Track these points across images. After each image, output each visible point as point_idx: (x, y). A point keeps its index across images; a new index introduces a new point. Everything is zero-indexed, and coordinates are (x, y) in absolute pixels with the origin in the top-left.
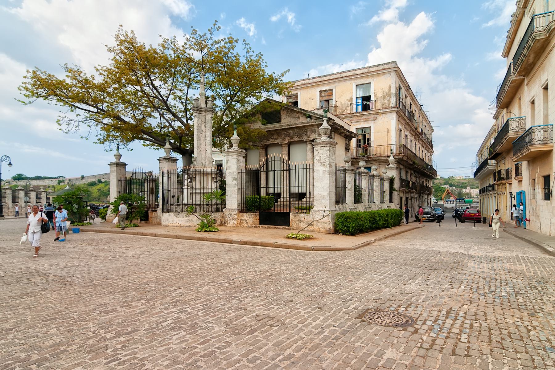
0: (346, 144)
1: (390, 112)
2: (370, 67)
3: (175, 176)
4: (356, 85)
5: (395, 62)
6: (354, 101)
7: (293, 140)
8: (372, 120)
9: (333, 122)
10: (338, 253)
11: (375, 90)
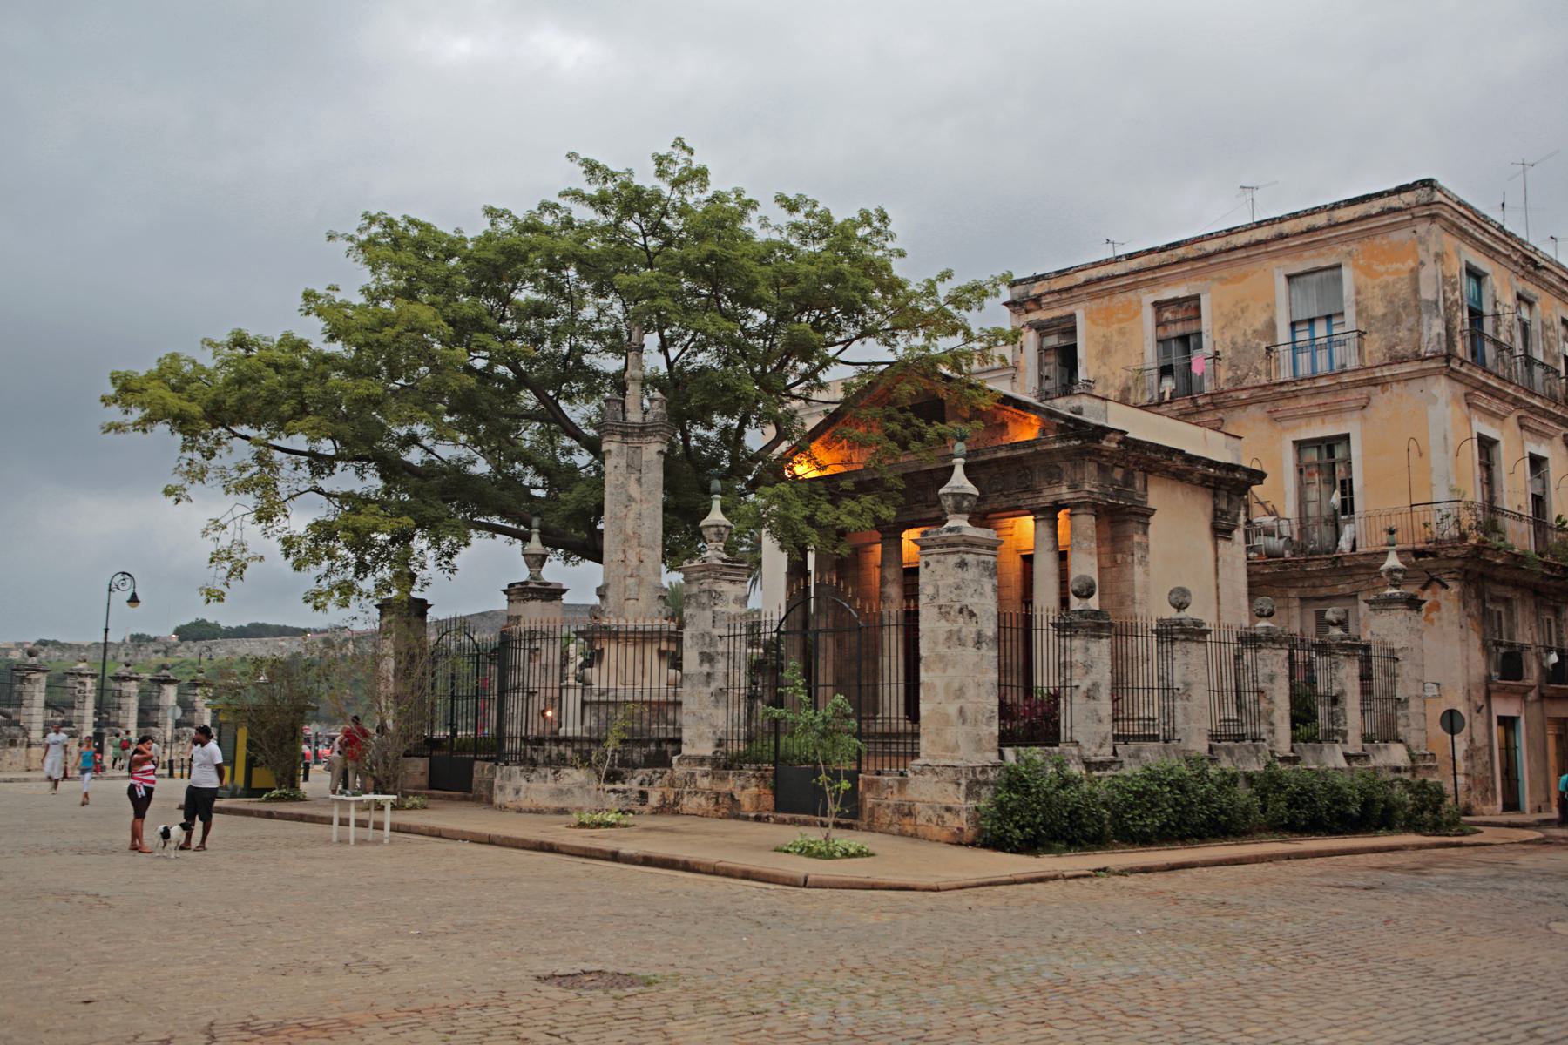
0: (1215, 510)
1: (1423, 375)
2: (1336, 206)
4: (1289, 278)
6: (1283, 334)
8: (1352, 409)
9: (1119, 437)
11: (1358, 293)
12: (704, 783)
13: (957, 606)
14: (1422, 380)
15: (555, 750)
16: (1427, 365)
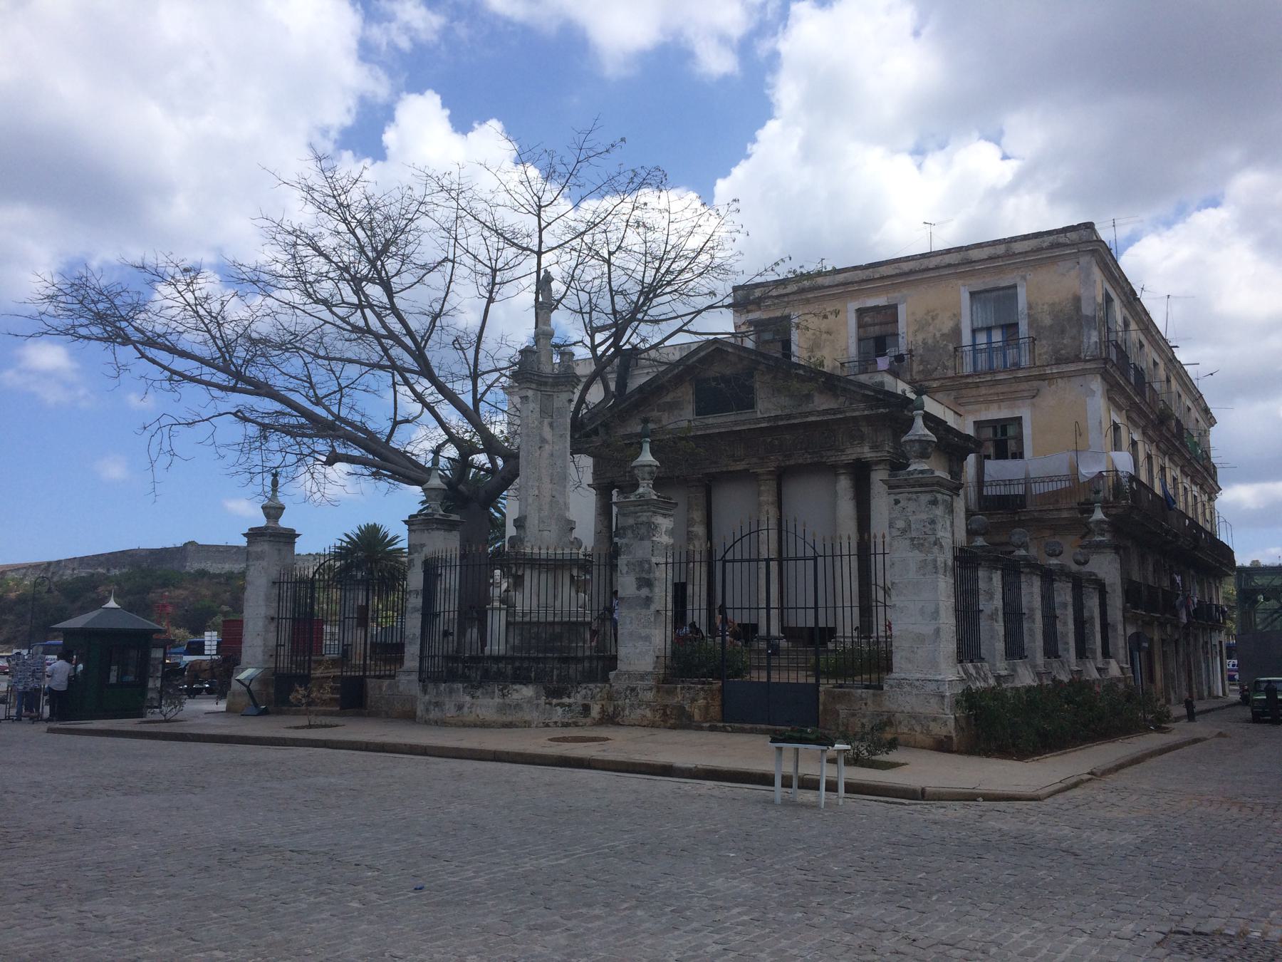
1: (1083, 373)
3: (453, 576)
4: (972, 294)
5: (1089, 226)
6: (966, 338)
7: (792, 462)
8: (1027, 398)
10: (1018, 804)
12: (650, 696)
13: (932, 539)
14: (1081, 378)
15: (495, 667)
16: (1088, 366)
